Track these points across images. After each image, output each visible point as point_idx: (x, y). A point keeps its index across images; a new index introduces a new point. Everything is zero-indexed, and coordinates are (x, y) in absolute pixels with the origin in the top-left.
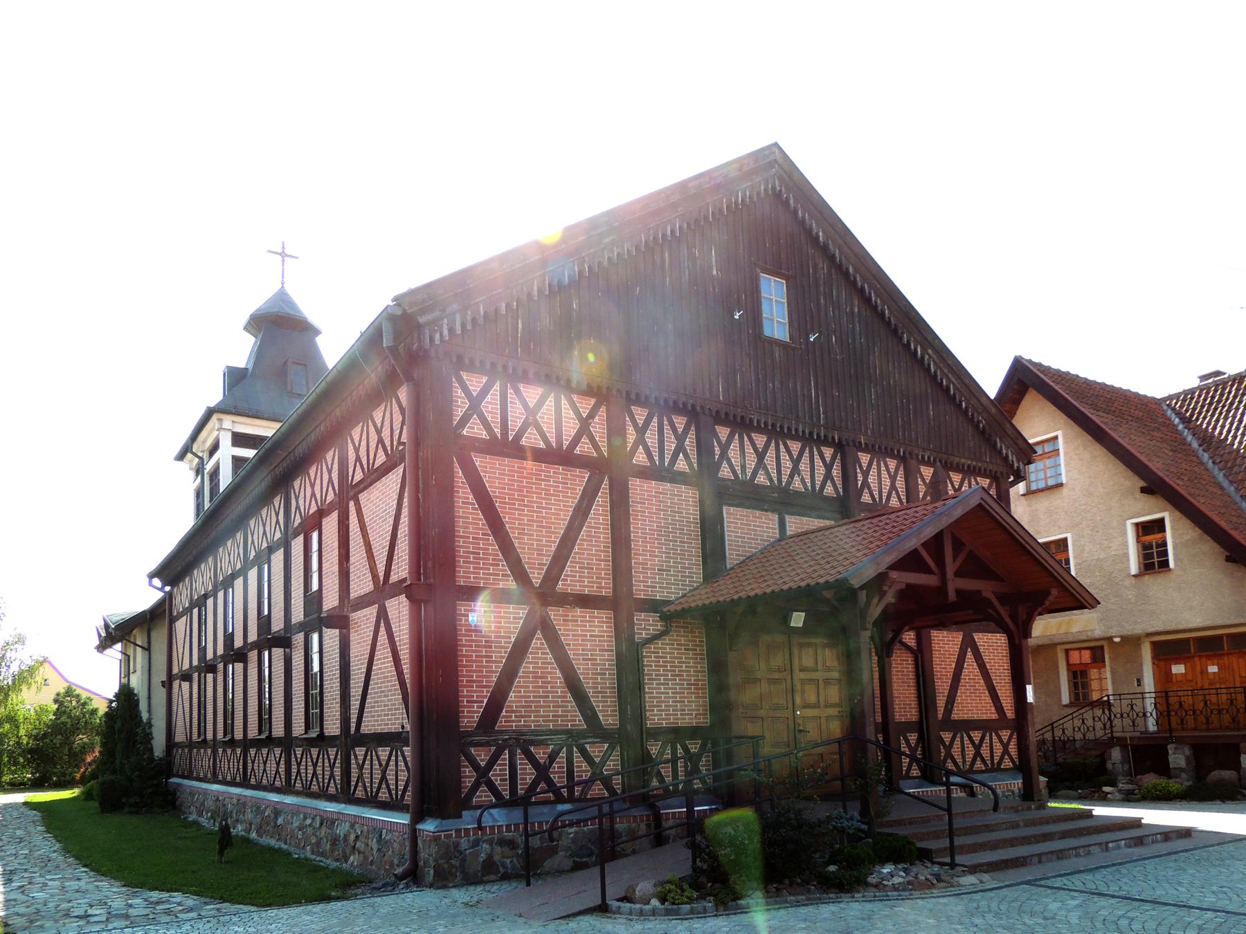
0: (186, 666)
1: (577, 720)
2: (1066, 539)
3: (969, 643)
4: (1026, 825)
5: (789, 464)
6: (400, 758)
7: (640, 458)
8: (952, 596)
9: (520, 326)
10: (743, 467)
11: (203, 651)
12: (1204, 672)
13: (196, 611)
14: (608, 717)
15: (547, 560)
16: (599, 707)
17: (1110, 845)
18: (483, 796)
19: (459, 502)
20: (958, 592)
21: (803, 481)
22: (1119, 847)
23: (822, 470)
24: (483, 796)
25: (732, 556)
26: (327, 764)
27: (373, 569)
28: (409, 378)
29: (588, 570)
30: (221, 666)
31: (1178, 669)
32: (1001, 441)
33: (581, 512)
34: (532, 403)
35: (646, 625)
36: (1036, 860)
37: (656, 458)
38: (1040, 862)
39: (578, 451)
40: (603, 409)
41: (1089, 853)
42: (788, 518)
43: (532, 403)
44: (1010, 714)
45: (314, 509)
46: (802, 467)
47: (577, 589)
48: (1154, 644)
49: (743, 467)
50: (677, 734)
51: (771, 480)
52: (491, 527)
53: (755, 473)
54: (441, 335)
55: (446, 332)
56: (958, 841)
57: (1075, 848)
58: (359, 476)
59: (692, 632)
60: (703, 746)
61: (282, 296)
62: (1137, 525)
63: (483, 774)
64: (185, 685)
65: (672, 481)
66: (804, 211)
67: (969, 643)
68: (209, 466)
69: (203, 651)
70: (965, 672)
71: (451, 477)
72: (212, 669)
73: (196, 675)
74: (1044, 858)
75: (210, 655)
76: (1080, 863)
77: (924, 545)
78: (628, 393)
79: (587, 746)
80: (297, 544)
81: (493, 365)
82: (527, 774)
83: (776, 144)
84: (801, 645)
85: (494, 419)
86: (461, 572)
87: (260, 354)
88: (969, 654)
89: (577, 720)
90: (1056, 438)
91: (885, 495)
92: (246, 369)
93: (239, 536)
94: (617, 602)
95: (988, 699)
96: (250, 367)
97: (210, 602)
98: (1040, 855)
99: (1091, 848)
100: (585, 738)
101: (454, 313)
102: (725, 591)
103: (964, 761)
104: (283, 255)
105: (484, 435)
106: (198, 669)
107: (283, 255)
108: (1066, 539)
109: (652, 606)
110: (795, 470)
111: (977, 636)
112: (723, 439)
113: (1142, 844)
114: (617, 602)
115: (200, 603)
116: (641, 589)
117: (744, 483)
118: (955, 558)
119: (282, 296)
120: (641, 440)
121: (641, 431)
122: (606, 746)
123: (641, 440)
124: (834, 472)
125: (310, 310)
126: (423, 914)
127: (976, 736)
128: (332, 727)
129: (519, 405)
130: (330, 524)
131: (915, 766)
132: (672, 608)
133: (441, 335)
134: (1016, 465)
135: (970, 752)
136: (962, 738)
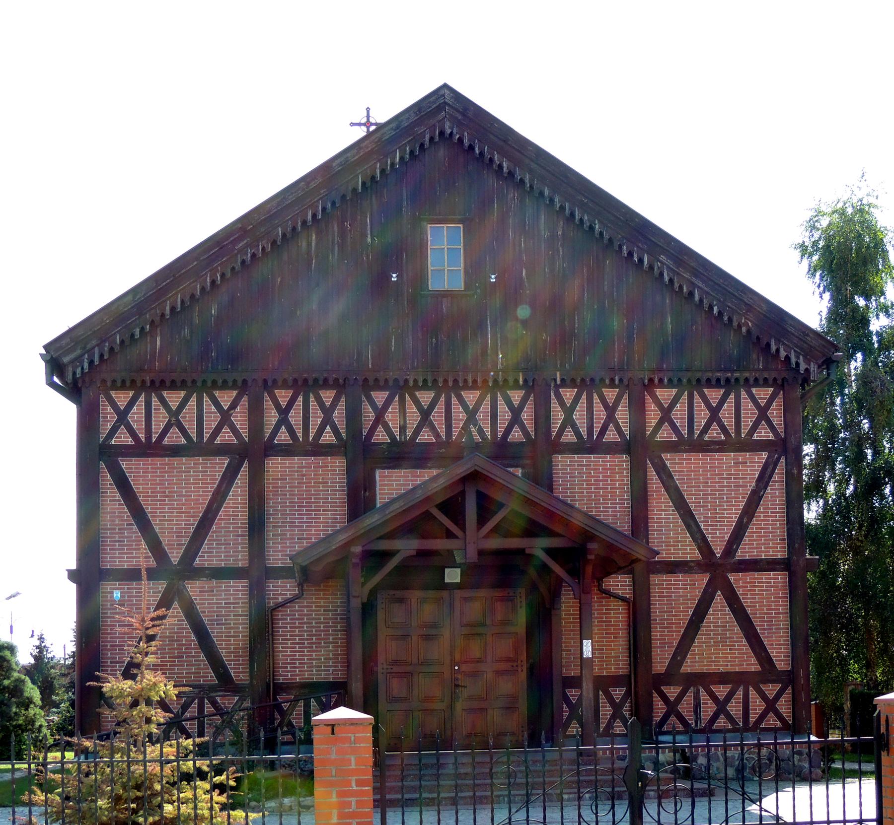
1: (750, 664)
5: (463, 416)
9: (158, 343)
10: (403, 429)
14: (239, 673)
15: (185, 541)
16: (773, 653)
23: (603, 415)
32: (778, 341)
34: (174, 405)
35: (281, 589)
40: (245, 398)
43: (174, 405)
47: (215, 563)
49: (403, 429)
50: (604, 683)
51: (437, 435)
52: (134, 516)
53: (508, 431)
54: (82, 368)
55: (86, 365)
59: (333, 594)
60: (628, 694)
65: (314, 454)
78: (265, 381)
79: (218, 699)
81: (680, 380)
82: (708, 708)
84: (466, 599)
85: (139, 426)
100: (216, 691)
101: (93, 348)
117: (402, 443)
122: (236, 698)
124: (372, 416)
129: (109, 409)
133: (82, 368)
134: (803, 367)
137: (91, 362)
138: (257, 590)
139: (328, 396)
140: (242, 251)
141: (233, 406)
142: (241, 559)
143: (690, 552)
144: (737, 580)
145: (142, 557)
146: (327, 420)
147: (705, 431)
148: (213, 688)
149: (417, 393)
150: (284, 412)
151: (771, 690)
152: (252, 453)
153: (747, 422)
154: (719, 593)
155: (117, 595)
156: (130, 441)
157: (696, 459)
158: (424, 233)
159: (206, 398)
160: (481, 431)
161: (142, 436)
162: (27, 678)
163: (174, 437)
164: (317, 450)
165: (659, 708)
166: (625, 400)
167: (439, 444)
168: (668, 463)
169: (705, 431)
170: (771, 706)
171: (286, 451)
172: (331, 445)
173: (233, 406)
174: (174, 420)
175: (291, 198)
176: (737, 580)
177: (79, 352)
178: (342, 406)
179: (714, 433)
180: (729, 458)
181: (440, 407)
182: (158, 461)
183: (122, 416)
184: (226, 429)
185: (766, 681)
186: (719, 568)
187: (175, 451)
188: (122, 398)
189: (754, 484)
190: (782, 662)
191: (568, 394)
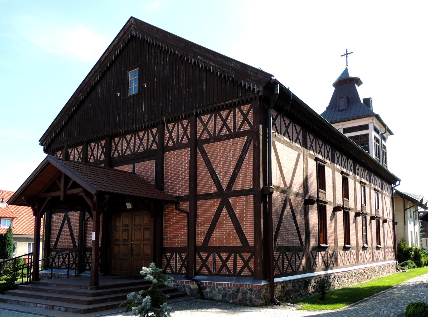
3: (66, 218)
4: (59, 293)
6: (297, 255)
7: (205, 136)
16: (248, 237)
17: (38, 305)
18: (204, 270)
21: (144, 147)
22: (42, 307)
24: (204, 270)
26: (346, 256)
36: (10, 302)
37: (179, 141)
38: (11, 303)
41: (29, 305)
44: (251, 243)
57: (24, 302)
63: (204, 262)
64: (386, 217)
67: (66, 218)
70: (220, 220)
74: (13, 302)
76: (19, 308)
77: (74, 181)
83: (131, 17)
88: (66, 223)
89: (237, 243)
95: (236, 235)
98: (11, 301)
99: (30, 304)
103: (214, 269)
113: (53, 309)
124: (168, 135)
126: (217, 313)
127: (224, 255)
131: (184, 269)
135: (219, 264)
136: (214, 256)
143: (214, 189)
145: (214, 189)
149: (221, 112)
151: (246, 255)
154: (225, 207)
155: (55, 218)
160: (144, 147)
165: (199, 262)
168: (205, 149)
170: (246, 264)
171: (207, 141)
172: (186, 144)
184: (225, 128)
185: (244, 251)
186: (224, 195)
189: (240, 153)
190: (251, 243)
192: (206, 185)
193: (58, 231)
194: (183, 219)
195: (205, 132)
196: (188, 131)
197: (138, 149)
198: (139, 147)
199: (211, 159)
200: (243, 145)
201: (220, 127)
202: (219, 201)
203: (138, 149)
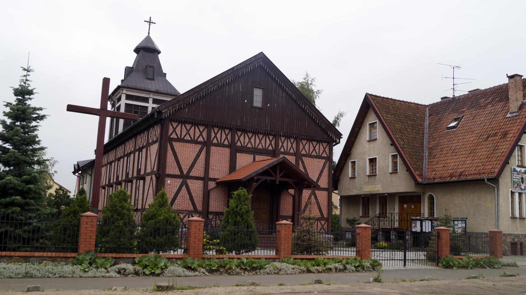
0: (104, 184)
2: (376, 158)
5: (258, 141)
7: (215, 141)
8: (278, 183)
10: (244, 142)
11: (110, 180)
12: (411, 207)
13: (109, 166)
15: (188, 168)
16: (197, 205)
19: (168, 154)
20: (280, 181)
21: (262, 146)
25: (238, 167)
27: (151, 166)
28: (161, 124)
29: (198, 171)
30: (114, 186)
31: (405, 206)
33: (198, 156)
34: (188, 128)
39: (199, 140)
42: (256, 156)
44: (326, 216)
45: (141, 146)
46: (262, 142)
48: (399, 197)
49: (244, 142)
51: (252, 145)
56: (140, 207)
58: (151, 141)
61: (148, 39)
62: (392, 155)
64: (103, 190)
65: (223, 147)
66: (269, 69)
68: (117, 105)
69: (110, 180)
71: (167, 146)
72: (112, 186)
73: (107, 187)
75: (112, 182)
80: (137, 153)
83: (262, 52)
86: (167, 170)
87: (137, 62)
89: (191, 208)
90: (376, 122)
91: (288, 149)
92: (132, 68)
93: (123, 146)
94: (205, 179)
95: (318, 211)
96: (135, 67)
97: (113, 164)
102: (235, 177)
104: (150, 22)
105: (176, 137)
106: (108, 185)
107: (150, 22)
108: (376, 158)
109: (214, 180)
110: (260, 143)
111: (316, 192)
112: (239, 135)
114: (205, 179)
115: (110, 163)
116: (211, 176)
118: (280, 174)
119: (148, 39)
120: (216, 137)
121: (216, 134)
123: (216, 137)
124: (273, 143)
125: (159, 44)
128: (140, 207)
129: (171, 127)
130: (144, 150)
132: (219, 181)
137: (170, 113)
138: (205, 185)
139: (202, 129)
140: (211, 88)
141: (203, 131)
142: (202, 175)
143: (177, 172)
144: (189, 182)
145: (177, 172)
146: (226, 138)
147: (312, 152)
148: (192, 212)
150: (314, 149)
151: (323, 222)
152: (207, 145)
153: (184, 134)
155: (169, 182)
156: (176, 137)
157: (310, 159)
158: (253, 90)
159: (196, 128)
160: (262, 146)
161: (179, 136)
162: (13, 197)
163: (187, 138)
164: (224, 146)
166: (295, 142)
167: (252, 148)
169: (312, 152)
171: (216, 145)
173: (203, 131)
174: (188, 133)
175: (224, 75)
176: (189, 182)
177: (167, 110)
178: (230, 134)
179: (314, 153)
180: (317, 160)
181: (286, 142)
182: (183, 144)
183: (201, 134)
184: (201, 137)
185: (322, 220)
186: (185, 177)
187: (187, 141)
188: (175, 125)
190: (326, 216)
191: (283, 139)
192: (171, 168)
193: (173, 194)
194: (291, 200)
195: (304, 150)
196: (237, 138)
197: (258, 146)
198: (259, 145)
199: (307, 167)
200: (323, 163)
201: (198, 135)
202: (181, 180)
203: (258, 146)
